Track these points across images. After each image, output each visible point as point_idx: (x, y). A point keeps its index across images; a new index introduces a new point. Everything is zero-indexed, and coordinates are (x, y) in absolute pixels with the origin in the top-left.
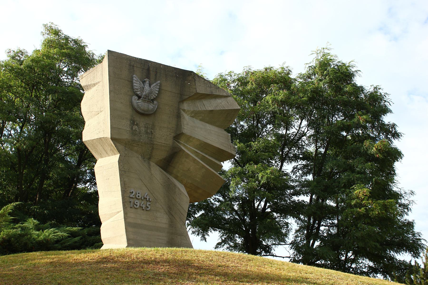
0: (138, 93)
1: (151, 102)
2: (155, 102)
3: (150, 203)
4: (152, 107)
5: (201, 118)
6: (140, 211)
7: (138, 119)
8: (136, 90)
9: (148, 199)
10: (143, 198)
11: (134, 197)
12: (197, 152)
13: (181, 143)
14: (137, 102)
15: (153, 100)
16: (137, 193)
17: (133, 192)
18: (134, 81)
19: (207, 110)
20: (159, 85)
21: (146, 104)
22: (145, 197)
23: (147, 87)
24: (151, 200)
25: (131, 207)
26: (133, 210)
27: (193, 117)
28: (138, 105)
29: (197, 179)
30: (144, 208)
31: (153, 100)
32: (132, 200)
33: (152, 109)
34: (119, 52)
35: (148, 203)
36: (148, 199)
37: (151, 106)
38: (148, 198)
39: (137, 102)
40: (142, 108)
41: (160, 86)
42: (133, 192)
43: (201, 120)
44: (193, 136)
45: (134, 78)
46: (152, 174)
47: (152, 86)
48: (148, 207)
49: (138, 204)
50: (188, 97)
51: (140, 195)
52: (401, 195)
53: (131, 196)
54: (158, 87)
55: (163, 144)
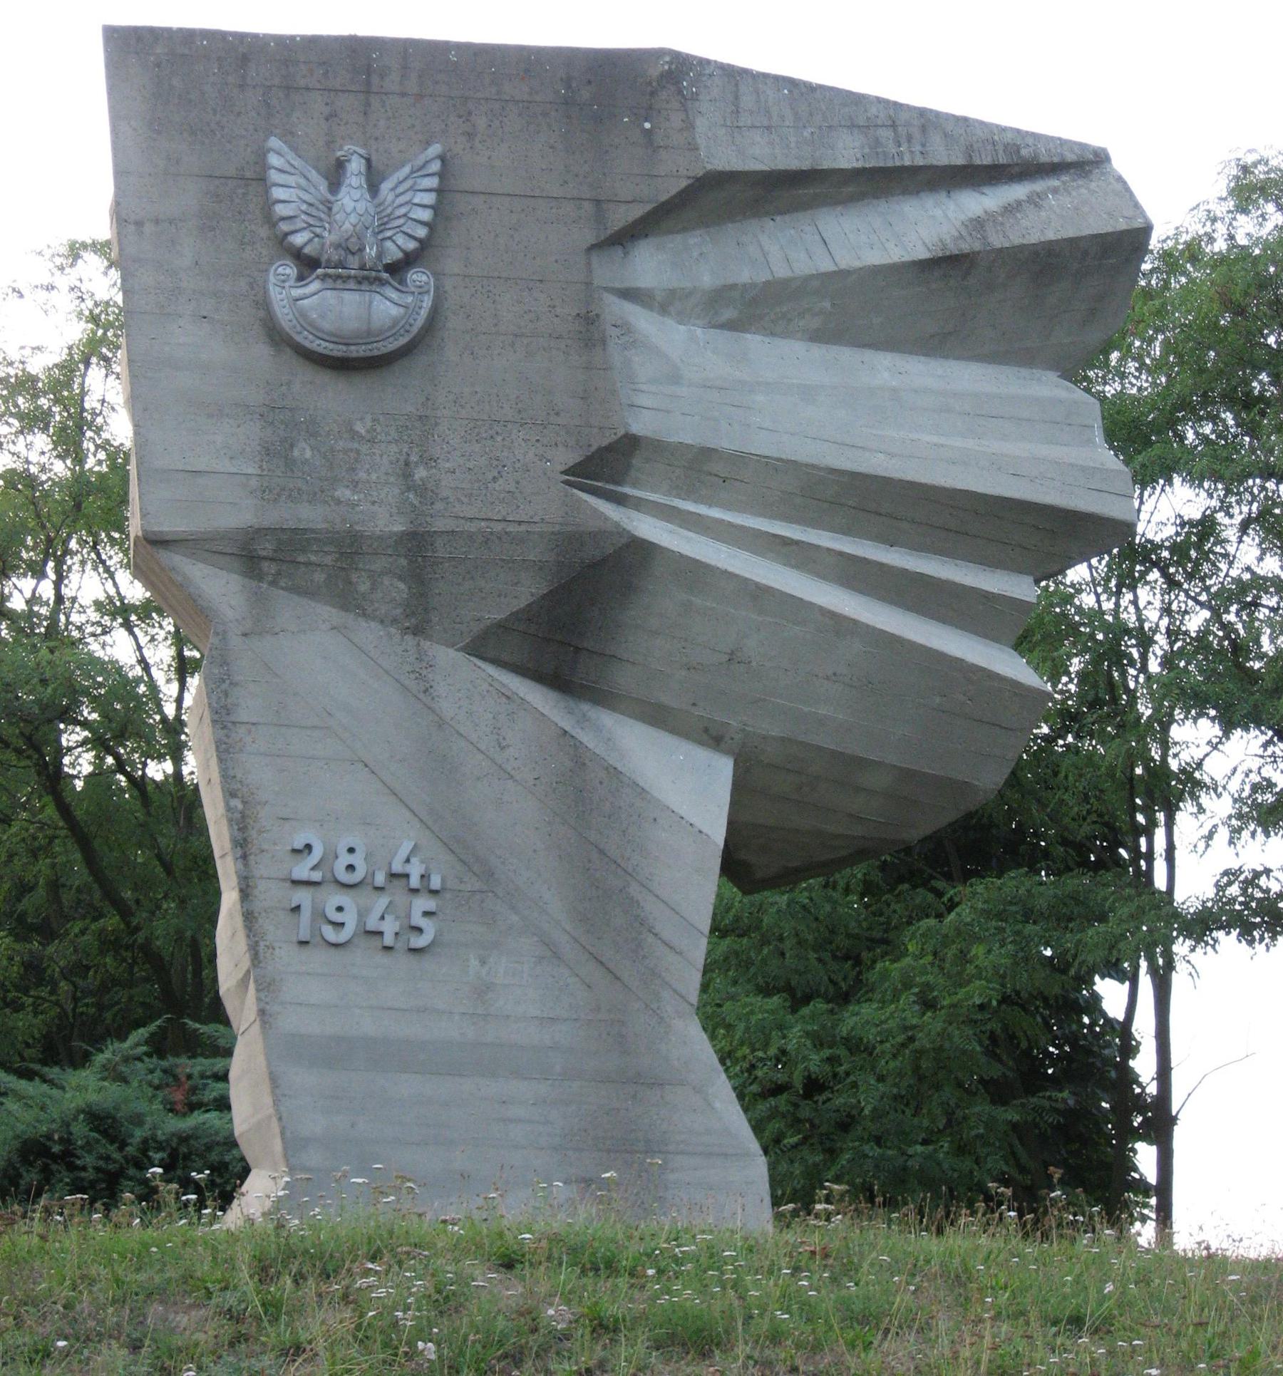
0: (299, 239)
1: (383, 283)
2: (417, 277)
3: (430, 904)
4: (395, 311)
5: (815, 323)
6: (364, 960)
7: (333, 399)
8: (284, 227)
9: (415, 882)
10: (380, 879)
11: (316, 876)
12: (786, 542)
13: (638, 505)
14: (296, 293)
15: (397, 269)
16: (342, 851)
17: (309, 847)
18: (274, 176)
19: (842, 274)
20: (435, 167)
21: (347, 296)
22: (397, 867)
23: (352, 200)
24: (436, 882)
25: (303, 943)
26: (318, 958)
27: (731, 326)
28: (303, 314)
29: (823, 711)
30: (388, 940)
31: (397, 269)
32: (302, 896)
33: (396, 321)
34: (854, 90)
35: (423, 903)
36: (415, 882)
37: (386, 308)
38: (415, 870)
39: (296, 293)
40: (326, 325)
41: (442, 175)
42: (309, 847)
43: (817, 337)
44: (727, 442)
45: (274, 160)
46: (441, 724)
47: (385, 187)
48: (419, 930)
49: (350, 918)
50: (637, 212)
51: (357, 860)
52: (809, 1076)
53: (302, 870)
54: (433, 182)
55: (498, 527)
